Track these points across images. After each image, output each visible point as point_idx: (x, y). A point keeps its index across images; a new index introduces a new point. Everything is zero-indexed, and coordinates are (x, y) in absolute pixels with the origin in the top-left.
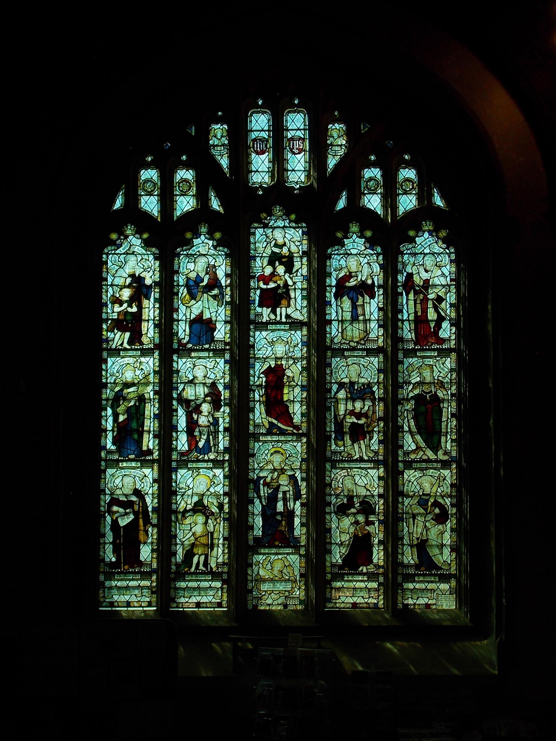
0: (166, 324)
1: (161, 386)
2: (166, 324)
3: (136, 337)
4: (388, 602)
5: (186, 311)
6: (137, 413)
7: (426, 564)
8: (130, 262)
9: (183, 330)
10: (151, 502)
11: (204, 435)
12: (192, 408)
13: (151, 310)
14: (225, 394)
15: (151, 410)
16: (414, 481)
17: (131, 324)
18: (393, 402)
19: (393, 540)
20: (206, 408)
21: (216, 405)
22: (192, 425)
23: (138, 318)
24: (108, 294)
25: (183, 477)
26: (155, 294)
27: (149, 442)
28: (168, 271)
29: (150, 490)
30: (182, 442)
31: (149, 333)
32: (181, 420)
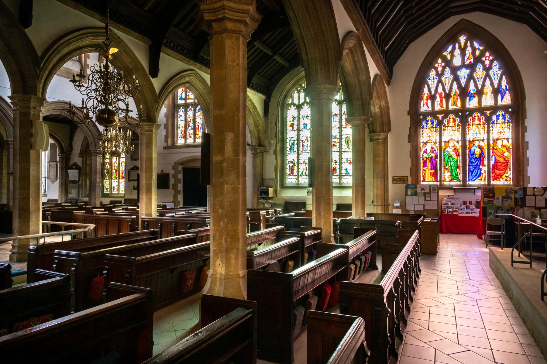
0: (298, 125)
1: (79, 48)
2: (298, 125)
3: (293, 128)
4: (288, 91)
5: (302, 122)
6: (293, 144)
7: (347, 173)
8: (291, 112)
9: (301, 127)
10: (296, 161)
11: (115, 154)
12: (303, 142)
13: (296, 122)
14: (309, 139)
15: (296, 142)
16: (344, 156)
17: (292, 126)
18: (341, 139)
19: (340, 168)
20: (306, 142)
21: (308, 141)
22: (303, 145)
23: (293, 124)
24: (288, 120)
25: (301, 156)
26: (297, 119)
27: (296, 149)
28: (299, 114)
29: (296, 159)
30: (301, 149)
31: (296, 127)
32: (301, 144)
